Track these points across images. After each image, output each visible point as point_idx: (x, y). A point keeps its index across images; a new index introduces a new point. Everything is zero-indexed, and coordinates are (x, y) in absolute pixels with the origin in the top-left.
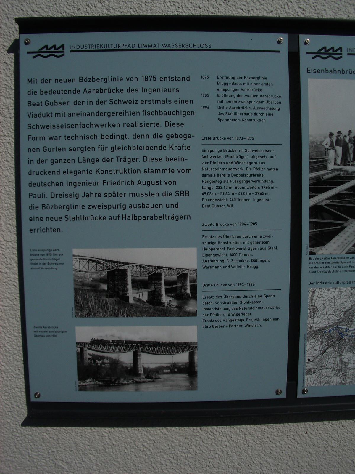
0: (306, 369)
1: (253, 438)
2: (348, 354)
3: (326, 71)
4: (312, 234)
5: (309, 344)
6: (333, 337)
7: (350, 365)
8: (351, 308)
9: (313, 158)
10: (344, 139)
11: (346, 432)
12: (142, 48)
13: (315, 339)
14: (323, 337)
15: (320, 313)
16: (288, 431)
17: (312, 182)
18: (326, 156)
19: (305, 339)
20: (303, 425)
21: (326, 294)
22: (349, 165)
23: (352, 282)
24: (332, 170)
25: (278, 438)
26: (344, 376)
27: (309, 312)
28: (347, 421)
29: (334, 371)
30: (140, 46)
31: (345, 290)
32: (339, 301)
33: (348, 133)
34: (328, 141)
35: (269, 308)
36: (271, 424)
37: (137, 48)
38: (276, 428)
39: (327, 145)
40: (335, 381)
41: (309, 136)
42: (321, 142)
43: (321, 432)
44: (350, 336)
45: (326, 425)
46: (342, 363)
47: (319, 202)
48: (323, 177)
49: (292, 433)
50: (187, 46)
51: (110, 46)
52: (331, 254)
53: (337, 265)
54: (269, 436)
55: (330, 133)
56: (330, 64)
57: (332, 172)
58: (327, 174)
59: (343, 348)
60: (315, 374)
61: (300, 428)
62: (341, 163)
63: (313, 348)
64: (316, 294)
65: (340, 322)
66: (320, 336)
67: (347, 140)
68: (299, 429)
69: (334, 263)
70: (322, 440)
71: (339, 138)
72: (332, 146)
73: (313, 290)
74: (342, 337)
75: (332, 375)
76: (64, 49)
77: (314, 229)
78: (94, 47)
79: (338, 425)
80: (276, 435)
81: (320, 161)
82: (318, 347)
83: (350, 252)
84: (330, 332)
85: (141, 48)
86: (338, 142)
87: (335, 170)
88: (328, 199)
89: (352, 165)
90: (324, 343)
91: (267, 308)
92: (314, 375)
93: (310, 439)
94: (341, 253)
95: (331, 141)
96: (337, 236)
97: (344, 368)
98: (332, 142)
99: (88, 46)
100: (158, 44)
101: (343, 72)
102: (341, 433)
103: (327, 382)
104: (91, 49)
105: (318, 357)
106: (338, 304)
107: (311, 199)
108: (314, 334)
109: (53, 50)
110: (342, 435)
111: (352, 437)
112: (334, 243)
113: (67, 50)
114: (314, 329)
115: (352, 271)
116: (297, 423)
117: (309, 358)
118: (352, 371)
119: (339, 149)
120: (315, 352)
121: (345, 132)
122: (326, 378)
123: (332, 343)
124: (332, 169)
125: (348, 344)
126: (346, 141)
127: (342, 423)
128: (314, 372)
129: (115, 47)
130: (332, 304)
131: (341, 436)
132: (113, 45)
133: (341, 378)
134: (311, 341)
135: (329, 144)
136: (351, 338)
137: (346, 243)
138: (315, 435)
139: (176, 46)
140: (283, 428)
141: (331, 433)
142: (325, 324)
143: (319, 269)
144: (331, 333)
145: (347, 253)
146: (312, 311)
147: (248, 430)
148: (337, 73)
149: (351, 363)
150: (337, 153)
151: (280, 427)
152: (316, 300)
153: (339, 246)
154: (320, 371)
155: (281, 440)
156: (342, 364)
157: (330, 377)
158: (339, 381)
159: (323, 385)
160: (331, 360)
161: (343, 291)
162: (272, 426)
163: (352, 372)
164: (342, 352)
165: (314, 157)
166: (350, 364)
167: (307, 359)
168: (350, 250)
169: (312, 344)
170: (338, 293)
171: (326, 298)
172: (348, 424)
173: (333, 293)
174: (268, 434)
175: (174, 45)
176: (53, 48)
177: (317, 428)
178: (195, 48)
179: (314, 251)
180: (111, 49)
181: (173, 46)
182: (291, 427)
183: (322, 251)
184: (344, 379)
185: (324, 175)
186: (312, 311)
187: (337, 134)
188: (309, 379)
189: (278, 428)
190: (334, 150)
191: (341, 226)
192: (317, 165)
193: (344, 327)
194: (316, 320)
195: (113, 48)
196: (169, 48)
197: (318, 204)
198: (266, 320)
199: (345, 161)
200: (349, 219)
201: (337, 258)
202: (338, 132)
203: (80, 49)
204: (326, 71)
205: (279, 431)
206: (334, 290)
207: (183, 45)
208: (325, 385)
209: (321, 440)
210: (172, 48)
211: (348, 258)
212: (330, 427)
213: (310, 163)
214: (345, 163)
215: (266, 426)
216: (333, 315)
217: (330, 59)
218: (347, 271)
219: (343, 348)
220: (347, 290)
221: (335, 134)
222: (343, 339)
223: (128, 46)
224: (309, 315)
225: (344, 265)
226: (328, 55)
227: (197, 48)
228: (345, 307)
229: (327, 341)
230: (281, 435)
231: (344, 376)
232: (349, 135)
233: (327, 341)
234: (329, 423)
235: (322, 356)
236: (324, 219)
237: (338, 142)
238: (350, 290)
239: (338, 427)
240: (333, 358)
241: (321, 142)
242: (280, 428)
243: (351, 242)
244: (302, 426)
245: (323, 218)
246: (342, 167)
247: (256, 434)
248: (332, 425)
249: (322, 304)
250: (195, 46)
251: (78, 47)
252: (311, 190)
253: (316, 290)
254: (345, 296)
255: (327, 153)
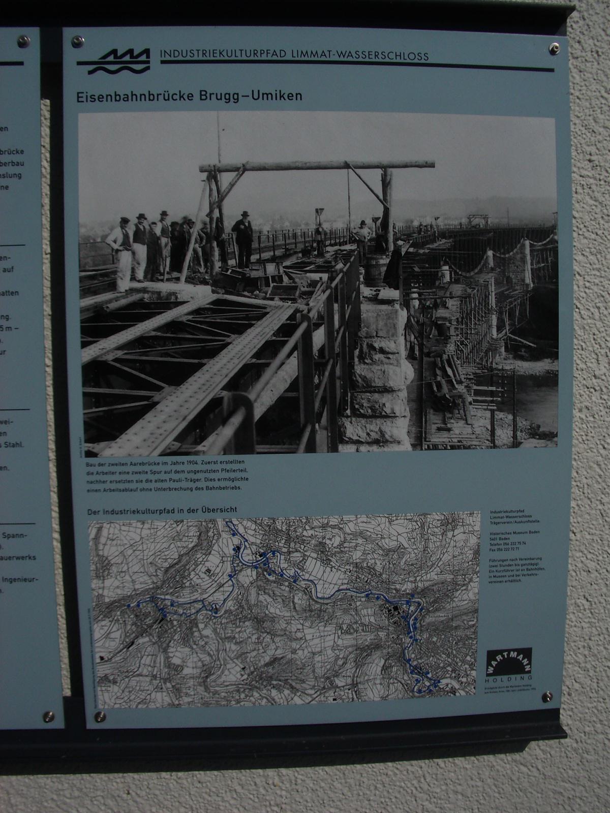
0: (99, 675)
1: (24, 800)
2: (179, 649)
3: (117, 97)
4: (89, 418)
5: (99, 628)
6: (147, 615)
7: (186, 671)
8: (180, 561)
9: (87, 268)
10: (151, 229)
11: (206, 793)
12: (299, 59)
13: (111, 619)
14: (126, 616)
15: (114, 569)
16: (90, 789)
17: (87, 315)
18: (113, 263)
19: (90, 618)
20: (119, 778)
21: (125, 533)
22: (162, 280)
23: (176, 511)
24: (126, 291)
25: (73, 800)
26: (177, 690)
27: (93, 567)
28: (208, 772)
29: (154, 681)
30: (295, 54)
31: (163, 527)
32: (152, 547)
33: (159, 217)
34: (118, 233)
35: (15, 558)
36: (56, 774)
37: (289, 57)
38: (67, 781)
39: (115, 242)
40: (160, 701)
41: (79, 225)
42: (105, 237)
43: (157, 792)
44: (181, 615)
45: (164, 778)
46: (169, 665)
47: (101, 356)
48: (108, 305)
49: (99, 793)
50: (383, 57)
51: (238, 53)
52: (129, 455)
53: (143, 477)
54: (55, 797)
55: (122, 218)
56: (125, 81)
57: (126, 294)
58: (117, 299)
59: (168, 637)
60: (118, 684)
61: (114, 784)
62: (145, 277)
63: (107, 636)
64: (105, 532)
65: (158, 588)
66: (118, 613)
67: (158, 231)
68: (113, 785)
69: (136, 473)
70: (160, 806)
71: (142, 227)
72: (126, 245)
73: (97, 526)
74: (165, 616)
75: (151, 688)
76: (148, 57)
77: (92, 408)
78: (207, 54)
79: (189, 780)
80: (68, 796)
81: (102, 275)
82: (117, 635)
83: (168, 451)
84: (138, 606)
85: (296, 59)
86: (139, 236)
87: (132, 291)
88: (119, 348)
89: (168, 280)
90: (129, 627)
91: (10, 558)
92: (116, 688)
93: (135, 805)
94: (150, 454)
95: (123, 234)
96: (141, 420)
97: (174, 674)
98: (126, 236)
99: (195, 53)
100: (329, 51)
101: (151, 97)
102: (197, 795)
103: (143, 701)
104: (201, 58)
105: (119, 652)
106: (151, 554)
107: (84, 349)
108: (108, 609)
109: (127, 58)
110: (199, 799)
111: (221, 803)
112: (136, 434)
113: (155, 59)
114: (107, 600)
115: (175, 489)
116: (107, 775)
117: (102, 655)
118: (191, 682)
119: (142, 250)
120: (113, 644)
121: (153, 215)
122: (141, 693)
123: (146, 627)
124: (127, 289)
125: (179, 630)
126: (155, 234)
127: (198, 776)
128: (115, 682)
129: (248, 55)
130: (139, 552)
131: (197, 801)
132: (244, 52)
133: (171, 694)
134: (103, 623)
135: (120, 241)
136: (183, 618)
137: (161, 435)
138: (146, 798)
139: (364, 57)
140: (81, 783)
141: (176, 795)
142: (128, 591)
143: (108, 486)
144: (141, 609)
145: (163, 454)
146: (98, 565)
147: (14, 786)
148: (139, 99)
149: (187, 667)
150: (137, 256)
151: (74, 780)
152: (105, 544)
153: (145, 440)
154: (127, 680)
155: (79, 804)
156: (169, 667)
157: (149, 692)
158: (167, 700)
159: (134, 707)
160: (147, 660)
161: (160, 528)
162: (59, 778)
163: (192, 683)
164: (168, 646)
165: (90, 267)
166: (185, 669)
167: (97, 656)
168: (169, 449)
169: (106, 628)
170: (148, 531)
171: (126, 542)
172: (210, 779)
173: (138, 531)
174: (52, 793)
175: (360, 54)
176: (129, 55)
177: (148, 784)
178: (398, 60)
179: (95, 451)
180: (239, 58)
181: (358, 56)
182: (96, 782)
183: (111, 451)
184: (176, 696)
185: (110, 301)
186: (98, 565)
187: (136, 221)
188: (106, 695)
189: (70, 782)
190: (130, 252)
191: (148, 400)
192: (96, 282)
193: (167, 597)
194: (108, 583)
195: (244, 58)
196: (350, 59)
197: (100, 359)
198: (12, 581)
199: (153, 272)
200: (163, 388)
201: (143, 464)
202: (138, 216)
203: (180, 58)
204: (117, 97)
205: (75, 789)
206: (141, 526)
207: (377, 54)
208: (140, 706)
209: (158, 807)
210: (355, 60)
211: (166, 463)
212: (175, 783)
213: (82, 279)
214: (153, 276)
215: (47, 778)
216: (143, 574)
217: (125, 73)
218: (164, 489)
219: (168, 637)
220: (167, 527)
221: (134, 220)
222: (167, 620)
223: (273, 55)
224: (93, 574)
225: (157, 477)
226: (95, 66)
227: (402, 61)
228: (166, 559)
229: (134, 624)
230: (79, 797)
231: (177, 690)
232: (162, 220)
233: (134, 624)
234: (171, 776)
235: (127, 651)
236: (113, 388)
237: (139, 236)
238: (175, 525)
239: (189, 784)
240: (150, 657)
241: (105, 237)
242: (75, 782)
243: (170, 433)
244: (118, 780)
245: (110, 386)
246: (147, 284)
247: (28, 793)
248: (177, 780)
249: (117, 553)
250: (398, 58)
251: (176, 53)
252: (85, 331)
253: (105, 525)
254: (164, 537)
255: (115, 257)
